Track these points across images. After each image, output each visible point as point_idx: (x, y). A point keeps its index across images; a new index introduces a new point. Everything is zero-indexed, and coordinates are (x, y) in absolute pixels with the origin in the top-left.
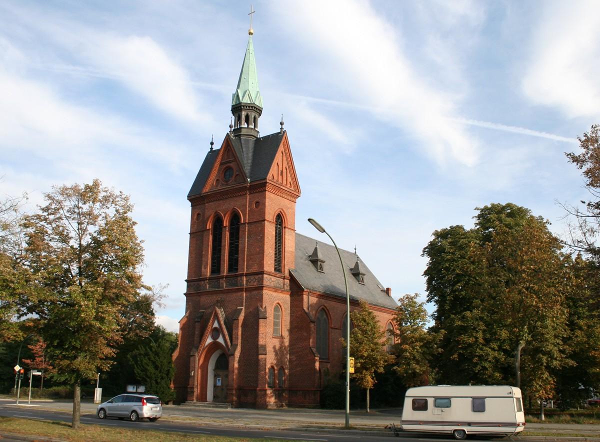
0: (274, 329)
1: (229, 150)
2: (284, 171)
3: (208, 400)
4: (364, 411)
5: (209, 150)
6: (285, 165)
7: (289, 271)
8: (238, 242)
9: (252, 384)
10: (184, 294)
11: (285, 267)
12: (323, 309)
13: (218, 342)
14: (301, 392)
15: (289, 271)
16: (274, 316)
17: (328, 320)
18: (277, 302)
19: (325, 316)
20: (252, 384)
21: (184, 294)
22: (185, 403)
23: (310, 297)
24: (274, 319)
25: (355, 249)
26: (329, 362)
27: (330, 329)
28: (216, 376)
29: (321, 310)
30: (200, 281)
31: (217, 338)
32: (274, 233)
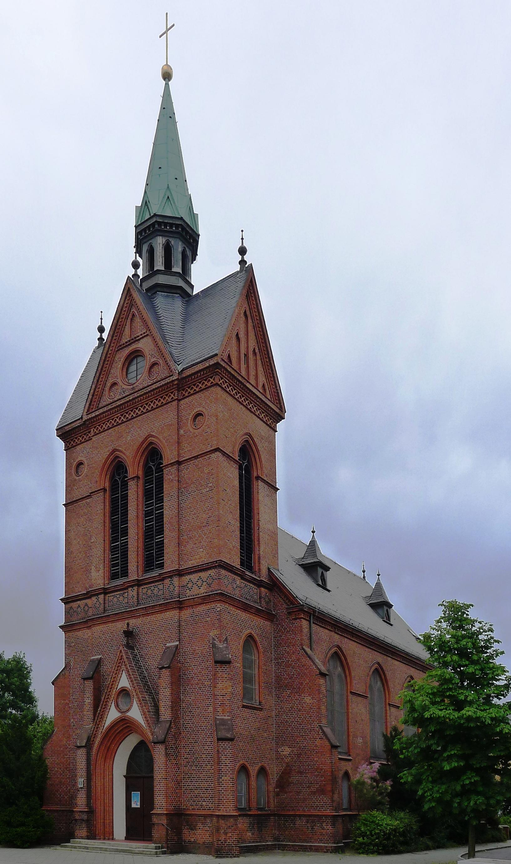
0: (244, 688)
1: (133, 315)
2: (251, 355)
3: (115, 836)
4: (107, 844)
5: (97, 343)
6: (252, 343)
7: (269, 569)
8: (162, 507)
9: (204, 803)
10: (61, 627)
11: (262, 562)
12: (336, 653)
13: (130, 718)
14: (304, 819)
15: (269, 569)
16: (244, 662)
17: (346, 677)
18: (248, 631)
19: (339, 669)
20: (204, 803)
21: (61, 627)
22: (69, 842)
23: (313, 625)
24: (244, 667)
25: (364, 572)
26: (350, 760)
27: (350, 696)
28: (129, 790)
29: (332, 656)
30: (90, 597)
31: (128, 710)
32: (237, 483)
